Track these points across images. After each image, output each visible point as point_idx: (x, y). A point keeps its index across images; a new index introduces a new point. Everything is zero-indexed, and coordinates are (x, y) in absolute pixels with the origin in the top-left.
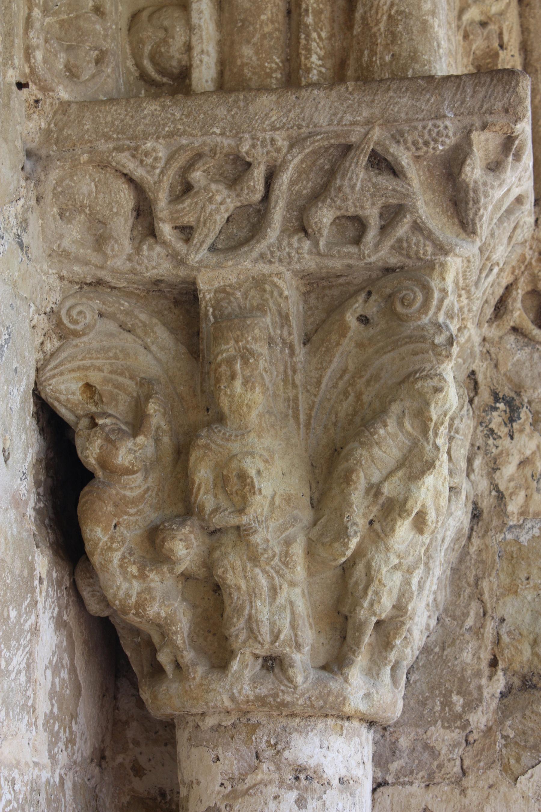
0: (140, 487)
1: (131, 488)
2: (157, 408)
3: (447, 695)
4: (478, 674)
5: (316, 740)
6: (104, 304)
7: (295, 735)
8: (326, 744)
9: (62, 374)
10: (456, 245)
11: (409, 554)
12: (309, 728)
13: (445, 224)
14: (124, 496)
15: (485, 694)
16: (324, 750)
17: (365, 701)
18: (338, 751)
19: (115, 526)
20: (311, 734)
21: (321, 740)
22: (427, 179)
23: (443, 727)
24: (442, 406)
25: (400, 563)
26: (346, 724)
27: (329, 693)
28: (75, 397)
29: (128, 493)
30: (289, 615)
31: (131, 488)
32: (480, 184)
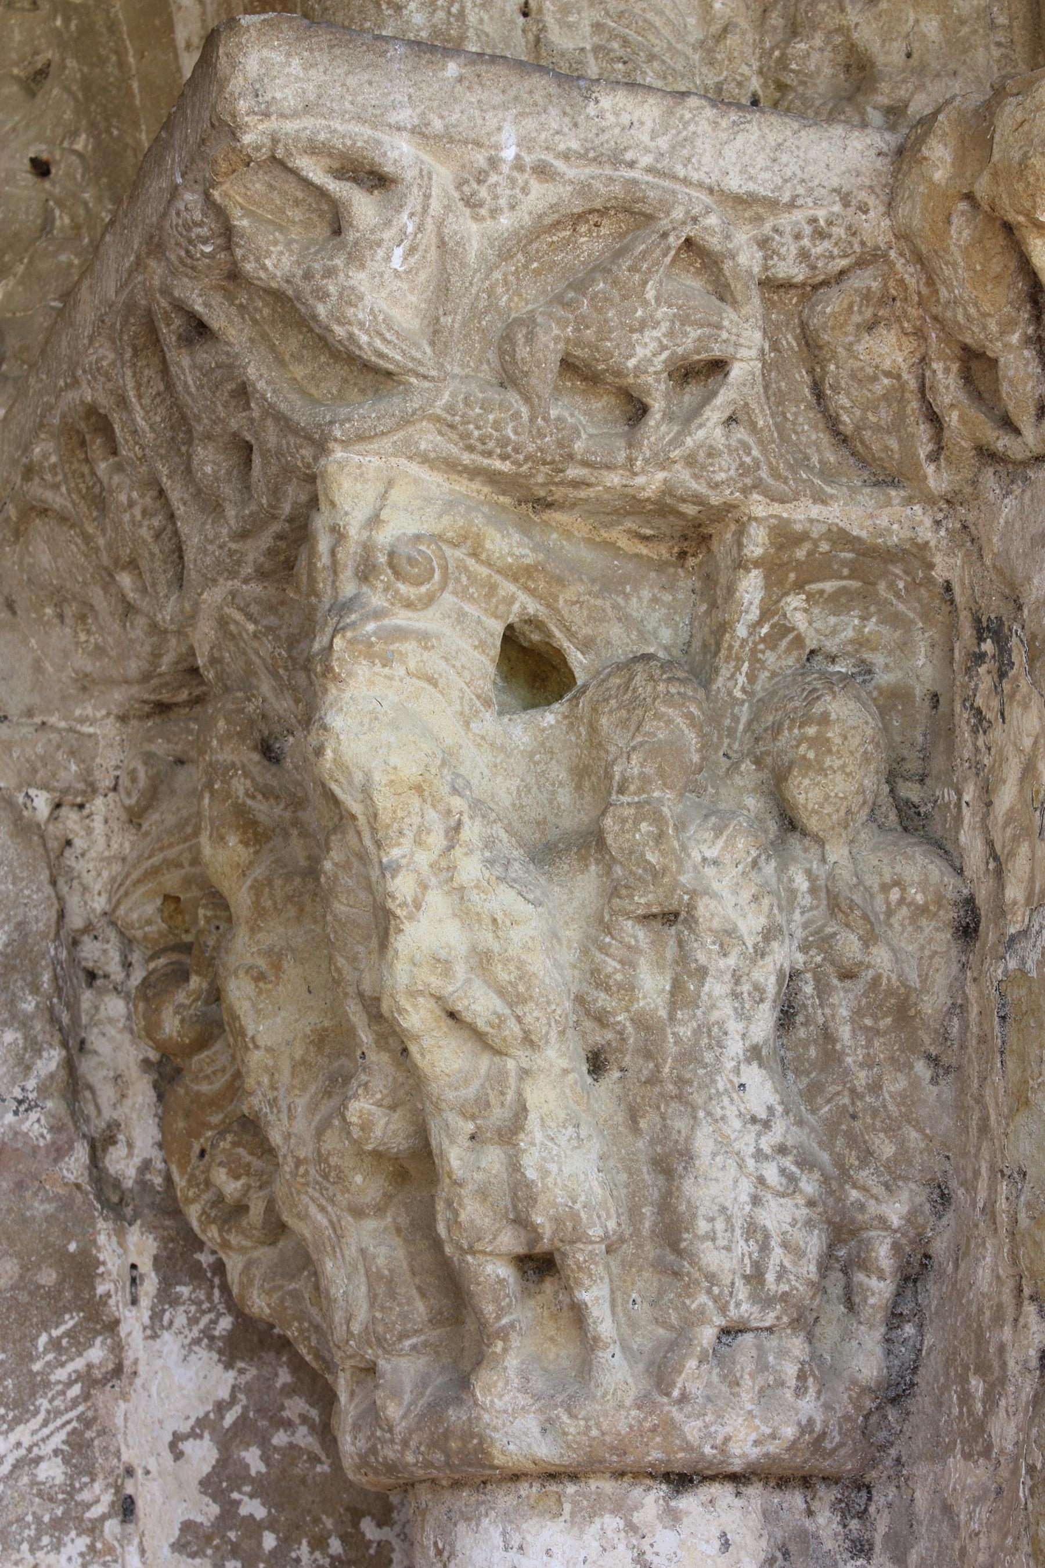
0: (223, 1070)
1: (207, 1077)
2: (209, 913)
3: (964, 1380)
4: (998, 1319)
5: (495, 1534)
6: (169, 741)
7: (462, 1527)
8: (516, 1540)
9: (126, 894)
10: (332, 423)
11: (488, 1104)
12: (482, 1509)
13: (346, 381)
14: (198, 1094)
15: (1011, 1363)
16: (512, 1555)
17: (550, 1437)
18: (548, 1552)
19: (202, 1153)
20: (485, 1522)
21: (504, 1533)
22: (274, 310)
23: (967, 1456)
24: (350, 782)
25: (478, 1127)
26: (571, 1489)
27: (447, 1435)
28: (155, 928)
29: (204, 1088)
30: (363, 1279)
31: (207, 1077)
32: (297, 280)
